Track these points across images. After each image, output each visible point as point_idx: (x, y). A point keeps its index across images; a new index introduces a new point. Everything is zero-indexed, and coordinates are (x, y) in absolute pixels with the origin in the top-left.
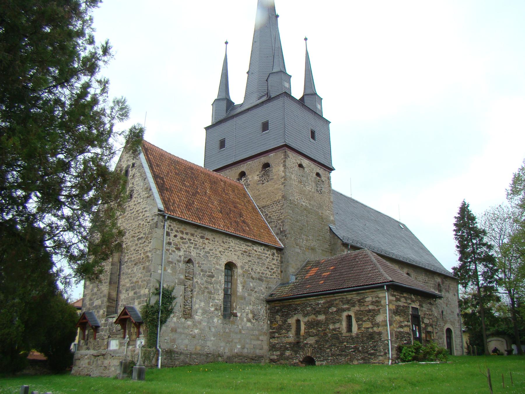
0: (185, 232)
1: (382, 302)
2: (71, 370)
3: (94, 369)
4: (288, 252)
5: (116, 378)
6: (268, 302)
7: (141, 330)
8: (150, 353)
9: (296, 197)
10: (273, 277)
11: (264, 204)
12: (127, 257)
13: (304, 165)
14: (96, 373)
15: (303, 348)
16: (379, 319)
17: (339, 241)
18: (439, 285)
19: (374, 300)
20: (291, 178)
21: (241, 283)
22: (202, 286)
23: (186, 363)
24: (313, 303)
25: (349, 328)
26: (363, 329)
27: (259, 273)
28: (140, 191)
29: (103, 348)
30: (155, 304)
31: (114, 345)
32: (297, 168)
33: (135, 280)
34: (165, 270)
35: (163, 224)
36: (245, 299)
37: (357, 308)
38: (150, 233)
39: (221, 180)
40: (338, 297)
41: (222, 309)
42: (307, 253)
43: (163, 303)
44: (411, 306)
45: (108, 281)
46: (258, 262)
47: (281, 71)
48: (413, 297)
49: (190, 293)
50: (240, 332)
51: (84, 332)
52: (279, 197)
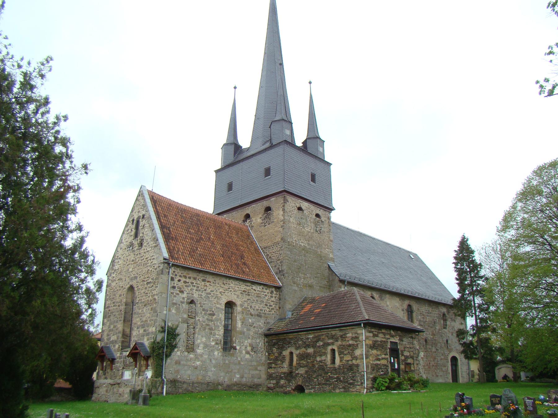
0: (188, 276)
1: (360, 338)
2: (92, 397)
3: (111, 396)
4: (285, 290)
5: (127, 403)
6: (266, 335)
7: (150, 363)
8: (156, 382)
9: (294, 239)
10: (271, 313)
11: (265, 245)
12: (138, 299)
13: (303, 208)
14: (112, 399)
15: (294, 378)
16: (357, 352)
17: (337, 278)
18: (444, 315)
19: (354, 336)
20: (289, 221)
21: (240, 320)
22: (204, 324)
23: (188, 391)
24: (304, 337)
25: (333, 361)
26: (344, 361)
27: (256, 309)
28: (149, 240)
29: (118, 377)
30: (161, 340)
31: (127, 375)
32: (296, 211)
33: (144, 319)
34: (170, 310)
35: (167, 270)
36: (244, 333)
37: (339, 343)
38: (157, 279)
39: (226, 223)
40: (324, 332)
41: (222, 343)
42: (304, 290)
43: (167, 339)
44: (389, 341)
45: (123, 319)
46: (257, 300)
47: (283, 120)
48: (392, 332)
49: (192, 330)
50: (239, 363)
51: (103, 364)
52: (278, 239)
